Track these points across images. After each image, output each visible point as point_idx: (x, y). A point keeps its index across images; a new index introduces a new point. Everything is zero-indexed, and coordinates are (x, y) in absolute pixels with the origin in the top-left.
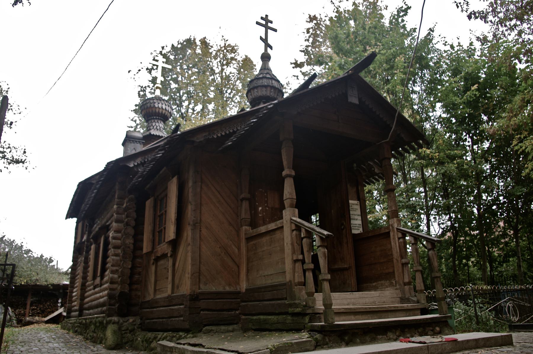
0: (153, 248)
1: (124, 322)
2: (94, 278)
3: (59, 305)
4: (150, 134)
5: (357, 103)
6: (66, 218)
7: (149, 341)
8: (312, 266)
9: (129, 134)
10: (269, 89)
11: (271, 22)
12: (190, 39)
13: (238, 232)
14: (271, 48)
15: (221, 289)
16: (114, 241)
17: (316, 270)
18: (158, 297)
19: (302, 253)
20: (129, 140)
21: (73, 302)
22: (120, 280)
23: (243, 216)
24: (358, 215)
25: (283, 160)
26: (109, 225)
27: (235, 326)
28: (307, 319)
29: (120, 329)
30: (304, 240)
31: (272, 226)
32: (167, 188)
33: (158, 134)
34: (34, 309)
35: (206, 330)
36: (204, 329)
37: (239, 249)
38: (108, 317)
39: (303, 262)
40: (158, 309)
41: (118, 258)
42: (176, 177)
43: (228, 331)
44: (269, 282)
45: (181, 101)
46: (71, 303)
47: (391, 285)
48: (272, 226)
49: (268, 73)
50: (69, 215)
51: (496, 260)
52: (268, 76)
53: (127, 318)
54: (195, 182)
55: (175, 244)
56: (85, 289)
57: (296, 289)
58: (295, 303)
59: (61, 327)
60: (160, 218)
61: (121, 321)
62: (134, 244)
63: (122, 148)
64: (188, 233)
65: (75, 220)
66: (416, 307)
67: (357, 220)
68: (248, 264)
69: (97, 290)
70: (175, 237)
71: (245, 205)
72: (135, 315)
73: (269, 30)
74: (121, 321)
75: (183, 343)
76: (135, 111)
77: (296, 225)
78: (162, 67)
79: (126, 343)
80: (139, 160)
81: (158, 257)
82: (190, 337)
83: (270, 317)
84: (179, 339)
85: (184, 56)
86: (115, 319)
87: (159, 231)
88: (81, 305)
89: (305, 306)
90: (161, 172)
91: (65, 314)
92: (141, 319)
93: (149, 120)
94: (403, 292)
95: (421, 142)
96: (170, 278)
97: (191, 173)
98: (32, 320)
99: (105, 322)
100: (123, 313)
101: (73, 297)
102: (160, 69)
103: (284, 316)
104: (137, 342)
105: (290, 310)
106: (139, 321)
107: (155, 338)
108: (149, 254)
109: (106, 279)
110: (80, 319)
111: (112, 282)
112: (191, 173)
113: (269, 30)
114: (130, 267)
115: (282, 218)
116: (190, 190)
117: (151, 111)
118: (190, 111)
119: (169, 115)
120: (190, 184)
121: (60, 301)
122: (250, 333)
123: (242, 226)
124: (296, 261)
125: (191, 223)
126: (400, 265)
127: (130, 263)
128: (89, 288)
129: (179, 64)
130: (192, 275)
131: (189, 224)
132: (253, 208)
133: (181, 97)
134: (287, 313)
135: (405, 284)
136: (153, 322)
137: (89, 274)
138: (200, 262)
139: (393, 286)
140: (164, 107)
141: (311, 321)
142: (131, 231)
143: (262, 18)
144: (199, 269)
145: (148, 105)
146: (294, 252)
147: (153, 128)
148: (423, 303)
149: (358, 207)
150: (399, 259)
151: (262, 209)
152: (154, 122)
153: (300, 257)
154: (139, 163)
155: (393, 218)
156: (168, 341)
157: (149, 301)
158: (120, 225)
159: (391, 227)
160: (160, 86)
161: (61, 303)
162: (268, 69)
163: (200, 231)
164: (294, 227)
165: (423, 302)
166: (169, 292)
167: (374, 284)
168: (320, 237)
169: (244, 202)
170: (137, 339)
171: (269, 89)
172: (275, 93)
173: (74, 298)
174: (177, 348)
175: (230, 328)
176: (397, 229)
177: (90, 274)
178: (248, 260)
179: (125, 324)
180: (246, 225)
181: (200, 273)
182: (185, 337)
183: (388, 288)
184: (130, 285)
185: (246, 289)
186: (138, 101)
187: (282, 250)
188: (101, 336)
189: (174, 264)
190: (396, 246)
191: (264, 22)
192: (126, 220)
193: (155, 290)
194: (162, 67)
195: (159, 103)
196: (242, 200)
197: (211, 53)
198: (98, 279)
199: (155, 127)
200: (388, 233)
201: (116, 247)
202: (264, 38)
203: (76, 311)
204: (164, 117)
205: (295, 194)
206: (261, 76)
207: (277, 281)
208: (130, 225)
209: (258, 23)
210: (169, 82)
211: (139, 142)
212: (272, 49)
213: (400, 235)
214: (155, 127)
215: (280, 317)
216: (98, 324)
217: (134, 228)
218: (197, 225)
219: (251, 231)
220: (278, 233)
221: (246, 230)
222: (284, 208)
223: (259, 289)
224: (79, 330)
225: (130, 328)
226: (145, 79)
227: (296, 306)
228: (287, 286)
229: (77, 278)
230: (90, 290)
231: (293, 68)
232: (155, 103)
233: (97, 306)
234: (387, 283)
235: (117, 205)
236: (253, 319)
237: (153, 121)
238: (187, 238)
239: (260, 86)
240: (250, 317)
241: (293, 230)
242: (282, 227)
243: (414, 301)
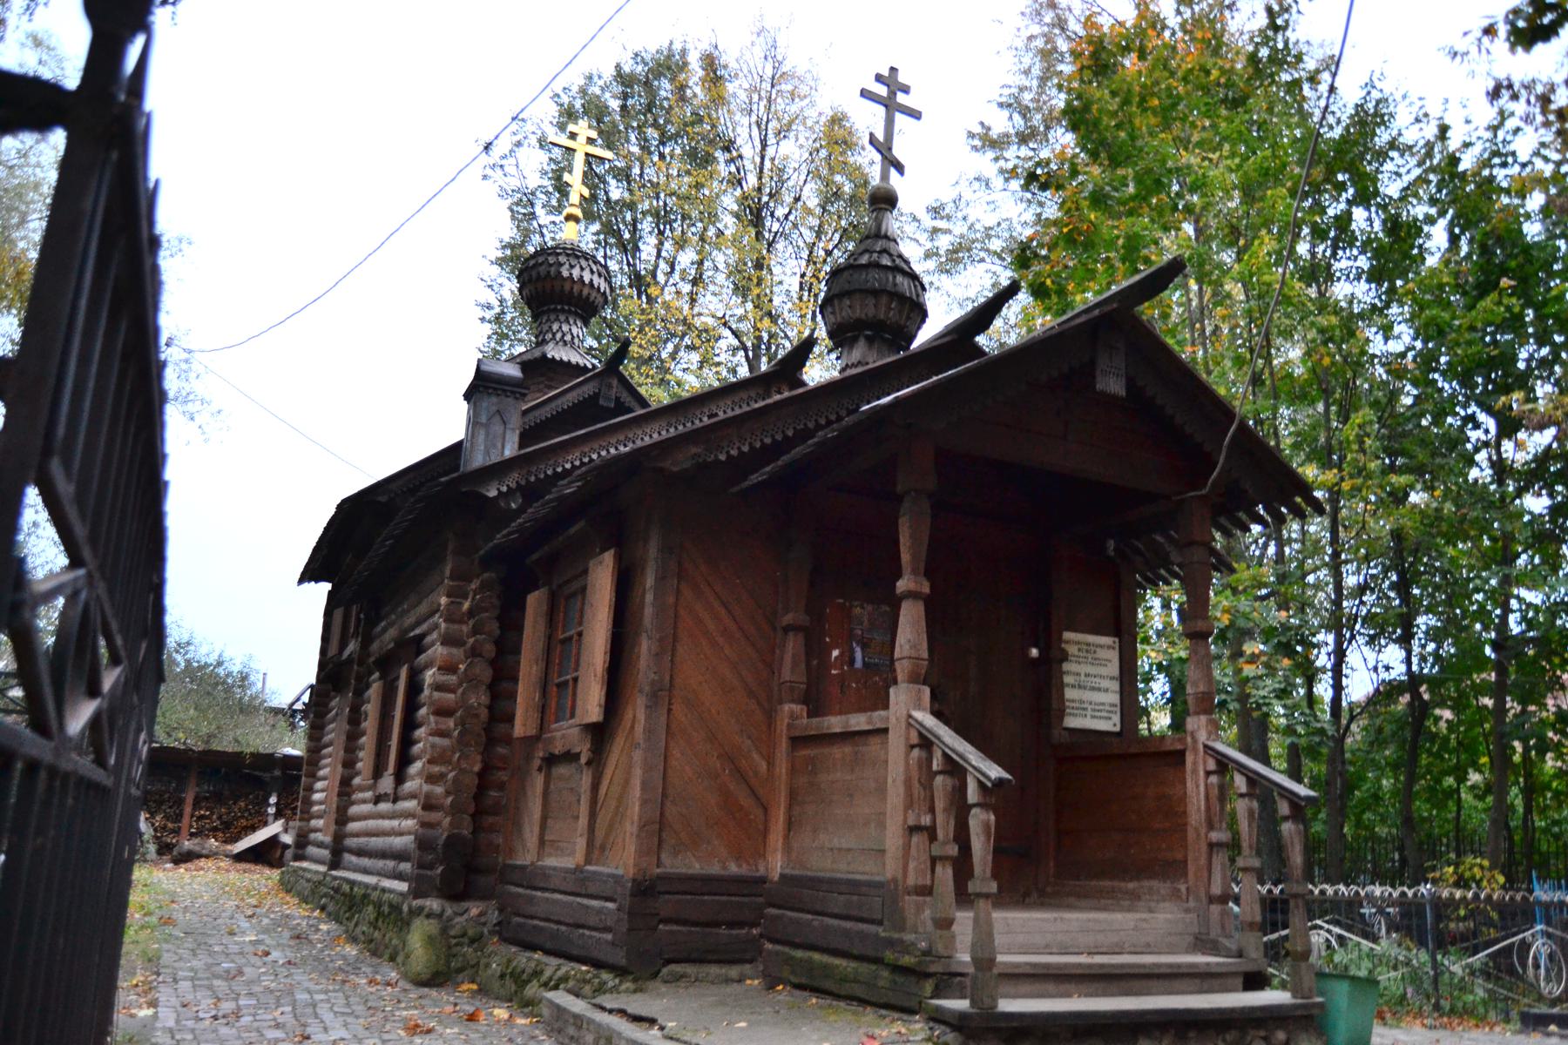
0: (542, 727)
1: (456, 914)
2: (377, 773)
3: (272, 810)
4: (544, 356)
5: (1123, 393)
6: (301, 581)
7: (520, 979)
8: (953, 850)
9: (483, 367)
10: (884, 299)
11: (906, 90)
12: (670, 56)
13: (770, 716)
14: (900, 168)
15: (715, 869)
16: (436, 695)
17: (963, 866)
18: (551, 862)
19: (932, 810)
20: (483, 386)
21: (312, 817)
22: (450, 799)
23: (787, 674)
24: (1112, 678)
25: (902, 549)
26: (423, 636)
27: (747, 968)
28: (929, 987)
29: (444, 931)
30: (939, 779)
31: (859, 722)
32: (586, 572)
33: (565, 359)
34: (201, 817)
35: (671, 973)
36: (665, 970)
37: (771, 764)
38: (415, 898)
39: (931, 832)
40: (547, 895)
41: (445, 742)
43: (728, 981)
44: (841, 869)
46: (308, 820)
47: (1175, 895)
48: (859, 722)
49: (885, 251)
50: (310, 574)
51: (1548, 787)
52: (886, 261)
53: (465, 905)
54: (661, 579)
55: (600, 733)
56: (349, 795)
57: (910, 901)
58: (902, 941)
59: (281, 882)
60: (562, 649)
61: (449, 912)
62: (490, 708)
64: (637, 712)
65: (325, 587)
66: (1233, 969)
67: (1106, 690)
68: (790, 807)
69: (384, 807)
70: (601, 719)
71: (792, 646)
72: (484, 897)
73: (898, 116)
74: (449, 912)
75: (608, 1006)
76: (500, 262)
77: (920, 734)
78: (587, 154)
79: (460, 970)
80: (512, 480)
81: (552, 755)
82: (627, 991)
83: (837, 961)
84: (600, 989)
86: (433, 904)
87: (557, 690)
88: (339, 838)
89: (927, 953)
91: (287, 839)
92: (501, 910)
93: (544, 312)
94: (1204, 920)
95: (1298, 500)
96: (583, 821)
97: (653, 551)
98: (197, 848)
99: (405, 908)
100: (458, 887)
101: (312, 804)
103: (874, 967)
104: (490, 972)
105: (889, 956)
106: (494, 916)
107: (537, 973)
108: (531, 741)
109: (409, 786)
110: (335, 878)
111: (429, 805)
112: (653, 551)
113: (898, 116)
114: (477, 768)
115: (886, 707)
116: (649, 597)
119: (600, 299)
120: (650, 581)
121: (273, 800)
122: (783, 993)
123: (781, 702)
124: (914, 829)
125: (647, 689)
126: (1204, 848)
127: (479, 758)
128: (361, 795)
130: (642, 827)
131: (641, 691)
132: (814, 650)
134: (878, 961)
135: (1212, 900)
136: (535, 927)
137: (361, 754)
138: (664, 795)
139: (1180, 897)
140: (587, 277)
141: (937, 994)
142: (485, 673)
143: (879, 78)
144: (662, 814)
145: (542, 269)
146: (909, 804)
148: (1255, 957)
149: (1114, 656)
150: (1203, 831)
151: (841, 654)
152: (557, 319)
153: (926, 820)
154: (513, 485)
155: (1198, 713)
156: (569, 991)
157: (523, 868)
158: (454, 651)
159: (1189, 739)
161: (277, 804)
162: (886, 237)
163: (669, 710)
164: (915, 739)
165: (1254, 955)
166: (579, 857)
167: (1131, 885)
168: (980, 782)
169: (791, 634)
170: (488, 965)
171: (884, 299)
172: (900, 312)
173: (316, 808)
174: (591, 1021)
175: (734, 971)
176: (1206, 746)
177: (365, 762)
178: (793, 796)
179: (458, 919)
180: (793, 701)
181: (662, 823)
182: (615, 990)
183: (1167, 904)
184: (476, 815)
185: (782, 876)
186: (509, 232)
187: (882, 790)
188: (395, 942)
189: (595, 787)
190: (1198, 794)
191: (882, 90)
192: (472, 640)
193: (542, 842)
194: (587, 154)
195: (572, 267)
196: (786, 630)
198: (386, 784)
199: (559, 336)
200: (1181, 754)
201: (442, 712)
202: (880, 136)
203: (320, 845)
204: (585, 306)
205: (925, 645)
206: (864, 260)
207: (860, 869)
208: (480, 655)
209: (865, 94)
212: (902, 173)
213: (1212, 765)
214: (559, 336)
215: (865, 969)
216: (386, 909)
217: (493, 663)
218: (661, 695)
219: (805, 721)
220: (875, 741)
221: (793, 716)
222: (895, 682)
223: (815, 883)
224: (331, 908)
225: (470, 932)
226: (533, 167)
227: (906, 948)
228: (889, 892)
229: (325, 751)
230: (364, 801)
231: (975, 148)
233: (383, 854)
234: (1163, 887)
235: (448, 596)
236: (792, 958)
237: (552, 317)
238: (632, 727)
239: (861, 291)
240: (787, 949)
241: (913, 747)
242: (886, 730)
243: (1229, 949)
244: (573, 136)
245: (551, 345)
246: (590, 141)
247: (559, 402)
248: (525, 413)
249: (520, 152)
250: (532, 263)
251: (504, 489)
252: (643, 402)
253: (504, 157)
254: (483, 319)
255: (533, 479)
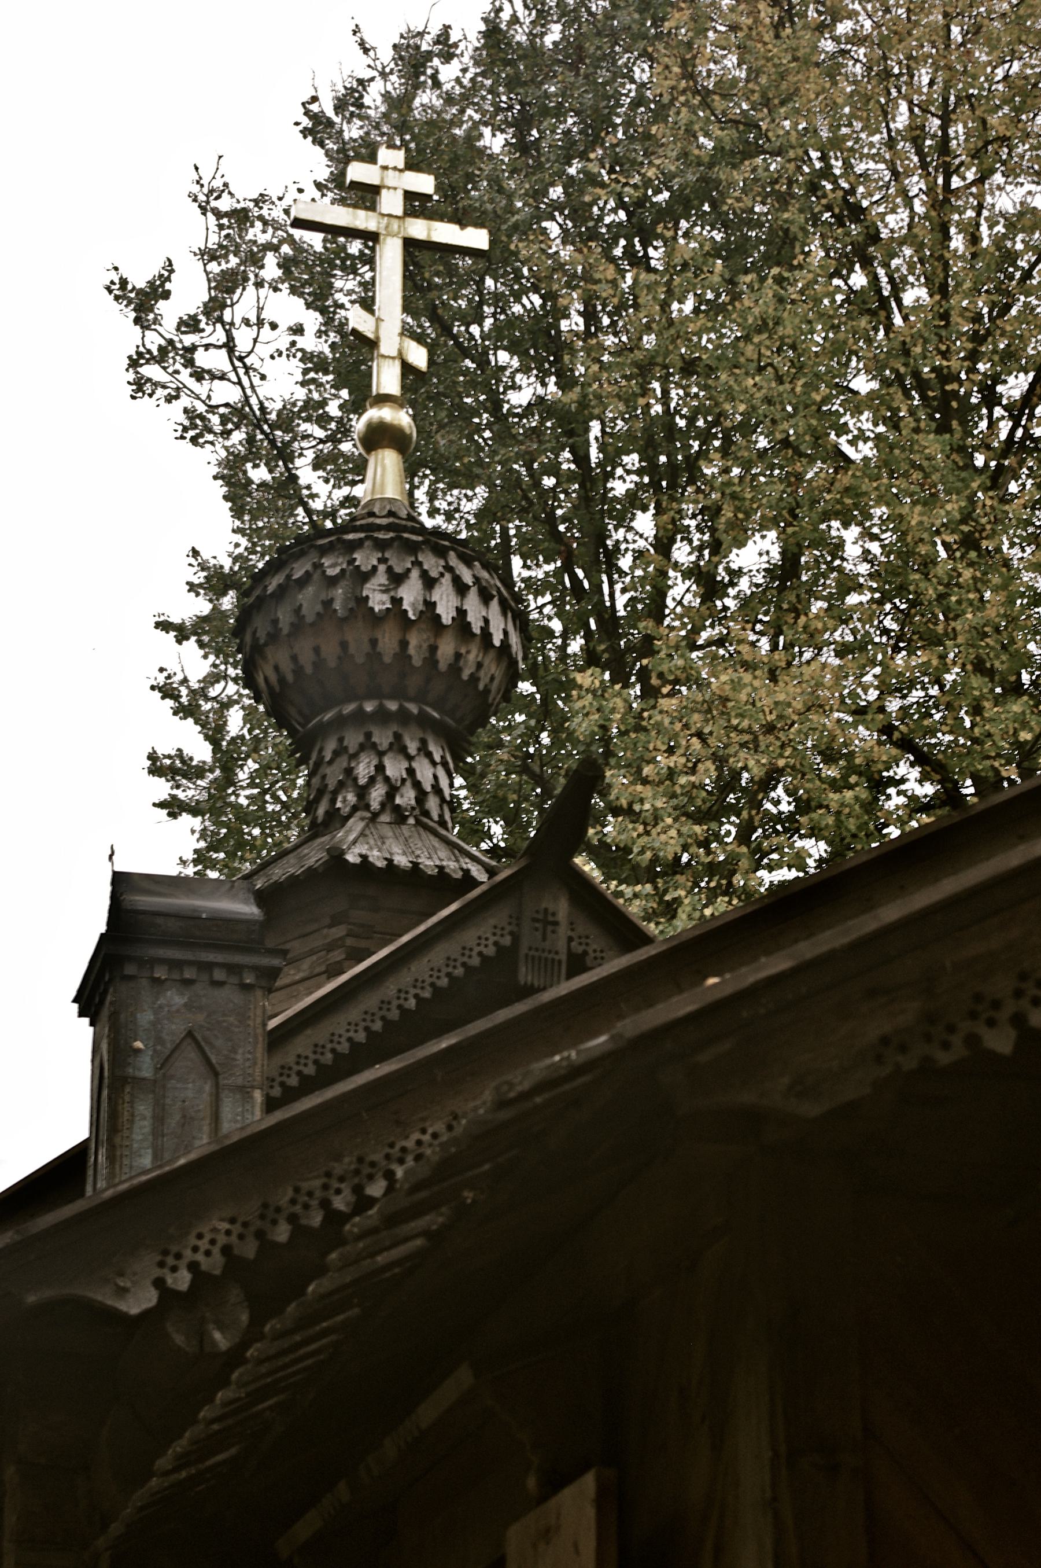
42: (588, 1482)
45: (597, 511)
63: (83, 1031)
78: (410, 245)
85: (597, 124)
90: (427, 1413)
102: (390, 258)
117: (330, 651)
118: (681, 591)
129: (556, 192)
133: (591, 481)
147: (362, 801)
154: (214, 1264)
160: (402, 418)
194: (410, 245)
195: (397, 579)
197: (833, 69)
199: (377, 795)
210: (483, 362)
211: (233, 969)
214: (377, 795)
232: (365, 577)
237: (353, 740)
244: (366, 196)
245: (356, 825)
246: (416, 205)
247: (390, 989)
248: (277, 1039)
249: (245, 303)
250: (274, 583)
251: (182, 1280)
252: (627, 934)
253: (190, 324)
254: (173, 807)
255: (282, 1233)
